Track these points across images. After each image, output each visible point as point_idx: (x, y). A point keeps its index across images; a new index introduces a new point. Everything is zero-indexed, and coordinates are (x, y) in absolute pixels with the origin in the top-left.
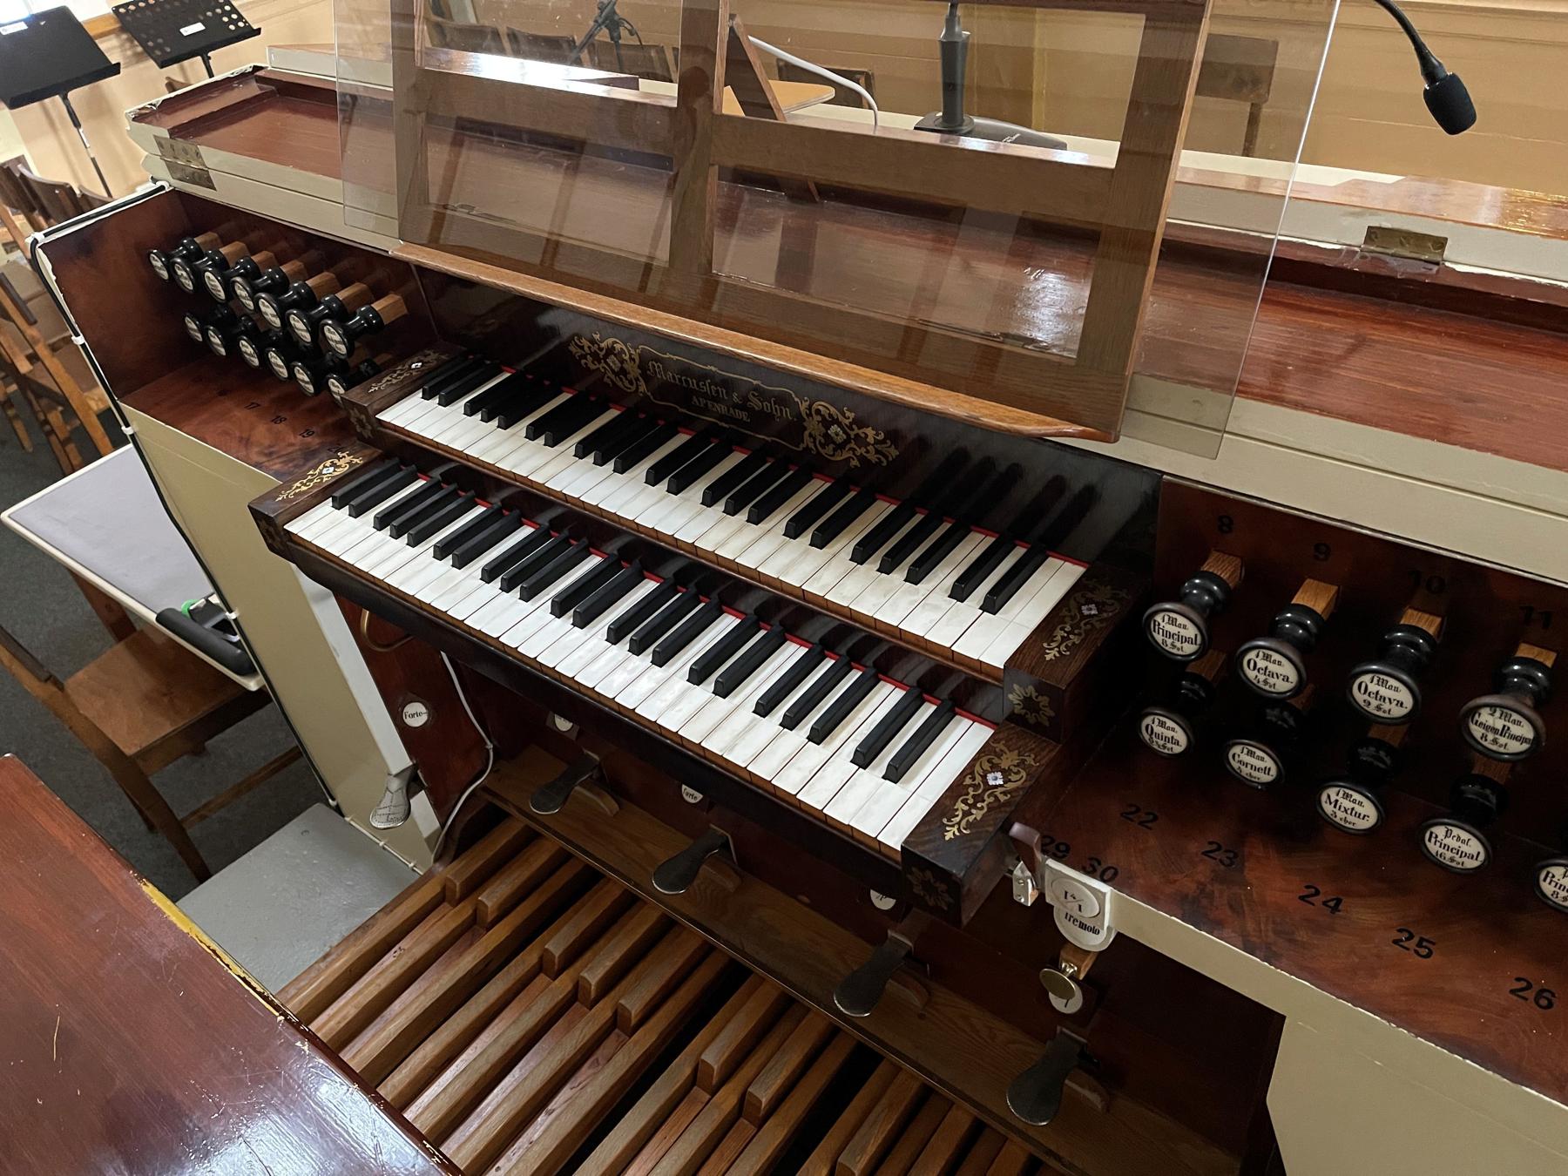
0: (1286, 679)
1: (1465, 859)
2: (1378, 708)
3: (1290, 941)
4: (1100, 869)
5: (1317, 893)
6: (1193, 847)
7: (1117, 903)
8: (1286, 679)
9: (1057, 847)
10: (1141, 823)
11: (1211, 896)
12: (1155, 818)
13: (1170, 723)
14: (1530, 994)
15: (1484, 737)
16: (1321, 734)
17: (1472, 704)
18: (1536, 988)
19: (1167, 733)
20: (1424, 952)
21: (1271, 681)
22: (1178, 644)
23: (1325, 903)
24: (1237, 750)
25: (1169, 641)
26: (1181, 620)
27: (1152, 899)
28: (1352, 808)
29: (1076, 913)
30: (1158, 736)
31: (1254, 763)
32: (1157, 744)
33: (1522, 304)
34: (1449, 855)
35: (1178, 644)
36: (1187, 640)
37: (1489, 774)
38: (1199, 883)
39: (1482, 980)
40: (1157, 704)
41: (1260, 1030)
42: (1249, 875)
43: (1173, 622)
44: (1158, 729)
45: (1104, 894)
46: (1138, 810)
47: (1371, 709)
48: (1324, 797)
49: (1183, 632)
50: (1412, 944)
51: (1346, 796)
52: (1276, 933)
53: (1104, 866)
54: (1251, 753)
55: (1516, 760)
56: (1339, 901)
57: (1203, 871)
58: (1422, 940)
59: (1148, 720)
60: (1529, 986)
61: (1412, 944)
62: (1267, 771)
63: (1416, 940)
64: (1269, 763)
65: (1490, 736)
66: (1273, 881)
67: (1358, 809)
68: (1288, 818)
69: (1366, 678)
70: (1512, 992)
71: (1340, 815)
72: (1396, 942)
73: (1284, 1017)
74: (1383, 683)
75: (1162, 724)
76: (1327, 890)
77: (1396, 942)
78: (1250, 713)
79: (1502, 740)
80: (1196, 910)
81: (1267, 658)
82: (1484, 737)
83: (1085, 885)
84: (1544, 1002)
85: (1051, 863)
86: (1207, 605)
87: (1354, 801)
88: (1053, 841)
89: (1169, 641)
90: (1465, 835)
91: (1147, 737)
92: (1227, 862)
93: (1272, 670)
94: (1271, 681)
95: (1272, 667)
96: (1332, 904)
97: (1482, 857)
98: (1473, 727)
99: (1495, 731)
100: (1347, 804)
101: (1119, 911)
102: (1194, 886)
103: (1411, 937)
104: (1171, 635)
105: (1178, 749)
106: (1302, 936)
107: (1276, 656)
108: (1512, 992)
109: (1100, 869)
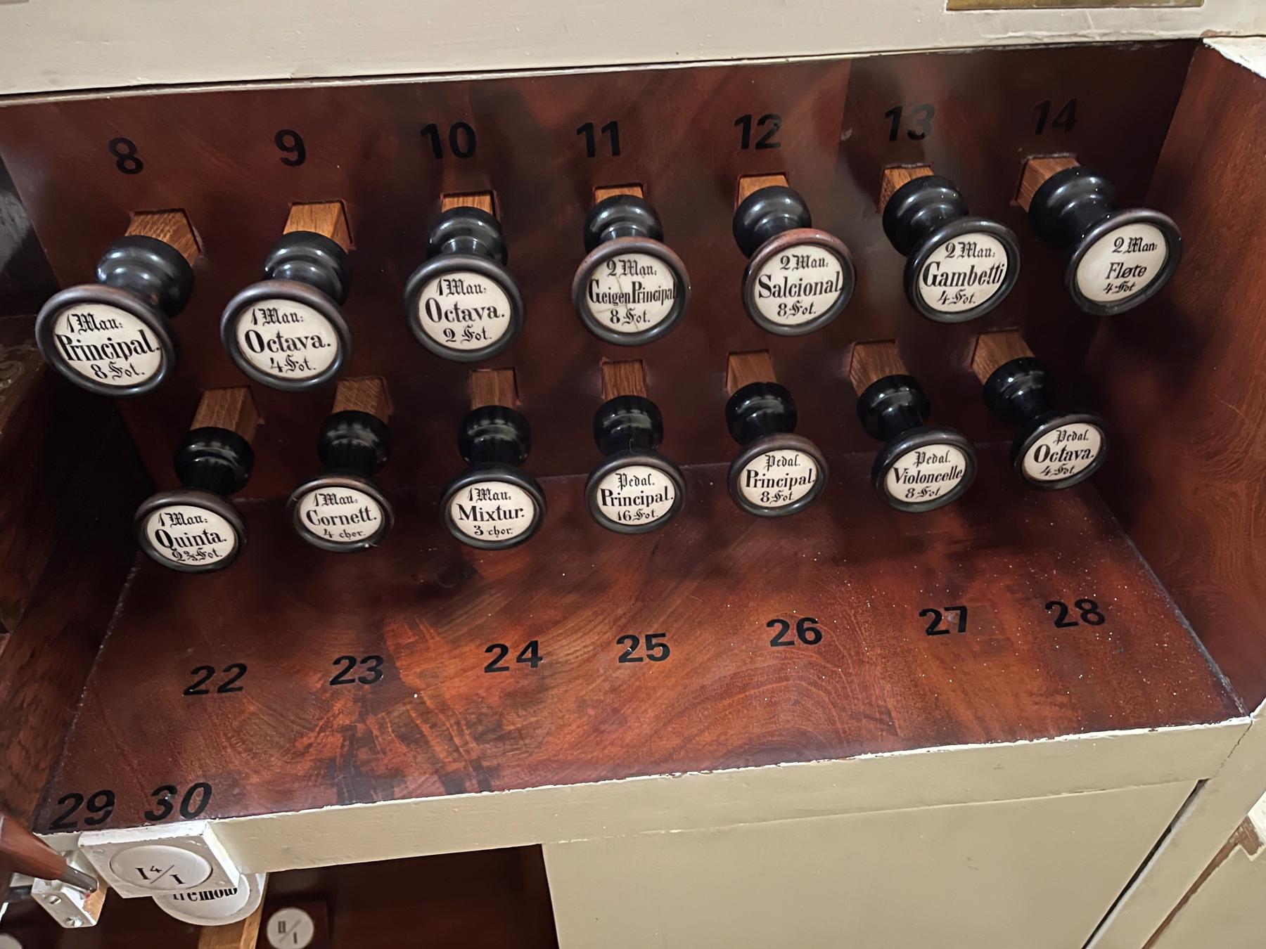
0: (318, 342)
1: (654, 506)
2: (468, 335)
3: (502, 738)
4: (177, 802)
5: (505, 650)
6: (316, 682)
7: (231, 837)
8: (318, 342)
9: (91, 807)
10: (222, 689)
11: (368, 739)
12: (243, 669)
13: (189, 512)
14: (792, 634)
15: (615, 316)
16: (413, 421)
17: (584, 266)
18: (793, 624)
19: (194, 532)
20: (658, 652)
21: (298, 356)
22: (121, 363)
23: (519, 659)
24: (307, 505)
25: (104, 364)
26: (101, 313)
27: (282, 797)
28: (495, 509)
29: (180, 889)
30: (181, 542)
31: (342, 512)
32: (190, 557)
33: (483, 361)
34: (633, 510)
35: (121, 363)
36: (126, 350)
37: (626, 391)
38: (343, 729)
39: (742, 648)
40: (154, 491)
41: (514, 881)
42: (410, 677)
43: (88, 323)
44: (176, 531)
45: (199, 838)
46: (211, 671)
47: (460, 344)
48: (456, 513)
49: (118, 336)
50: (641, 651)
51: (483, 494)
52: (478, 738)
53: (182, 791)
54: (330, 499)
55: (671, 325)
56: (534, 646)
57: (343, 709)
58: (649, 638)
59: (153, 525)
60: (786, 626)
61: (641, 651)
62: (364, 514)
63: (642, 641)
64: (363, 501)
65: (622, 310)
66: (443, 667)
67: (506, 505)
68: (422, 567)
69: (431, 292)
70: (774, 642)
71: (487, 526)
72: (624, 658)
73: (540, 846)
74: (457, 288)
75: (178, 519)
76: (513, 640)
77: (624, 658)
78: (300, 433)
79: (638, 309)
80: (356, 775)
81: (271, 316)
82: (615, 316)
83: (160, 842)
84: (810, 636)
85: (89, 839)
86: (150, 286)
87: (496, 497)
88: (79, 798)
89: (104, 364)
90: (642, 472)
91: (167, 552)
92: (371, 675)
93: (291, 337)
94: (298, 356)
95: (290, 331)
96: (529, 654)
97: (671, 493)
98: (595, 307)
99: (624, 298)
100: (487, 506)
101: (245, 848)
102: (337, 739)
103: (636, 642)
104: (100, 352)
105: (225, 548)
106: (514, 721)
107: (285, 307)
108: (774, 642)
109: (177, 802)
